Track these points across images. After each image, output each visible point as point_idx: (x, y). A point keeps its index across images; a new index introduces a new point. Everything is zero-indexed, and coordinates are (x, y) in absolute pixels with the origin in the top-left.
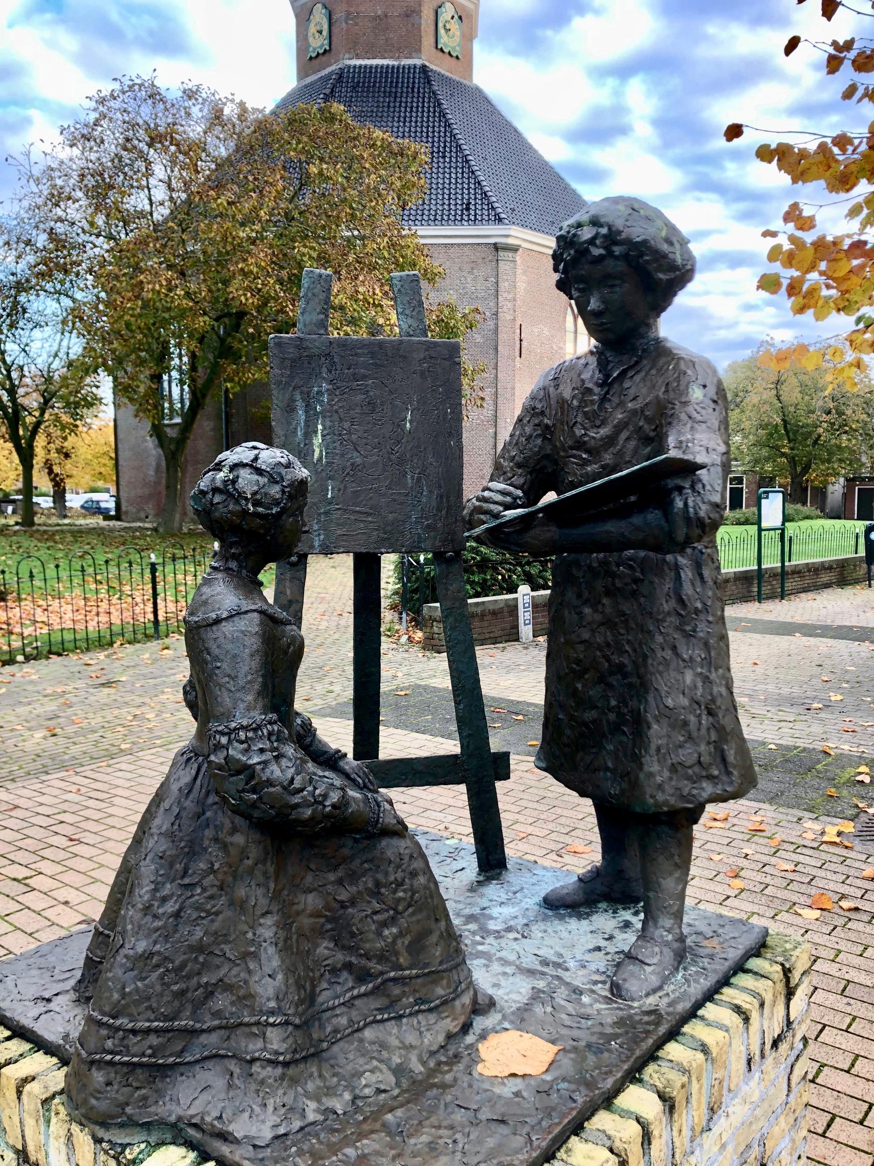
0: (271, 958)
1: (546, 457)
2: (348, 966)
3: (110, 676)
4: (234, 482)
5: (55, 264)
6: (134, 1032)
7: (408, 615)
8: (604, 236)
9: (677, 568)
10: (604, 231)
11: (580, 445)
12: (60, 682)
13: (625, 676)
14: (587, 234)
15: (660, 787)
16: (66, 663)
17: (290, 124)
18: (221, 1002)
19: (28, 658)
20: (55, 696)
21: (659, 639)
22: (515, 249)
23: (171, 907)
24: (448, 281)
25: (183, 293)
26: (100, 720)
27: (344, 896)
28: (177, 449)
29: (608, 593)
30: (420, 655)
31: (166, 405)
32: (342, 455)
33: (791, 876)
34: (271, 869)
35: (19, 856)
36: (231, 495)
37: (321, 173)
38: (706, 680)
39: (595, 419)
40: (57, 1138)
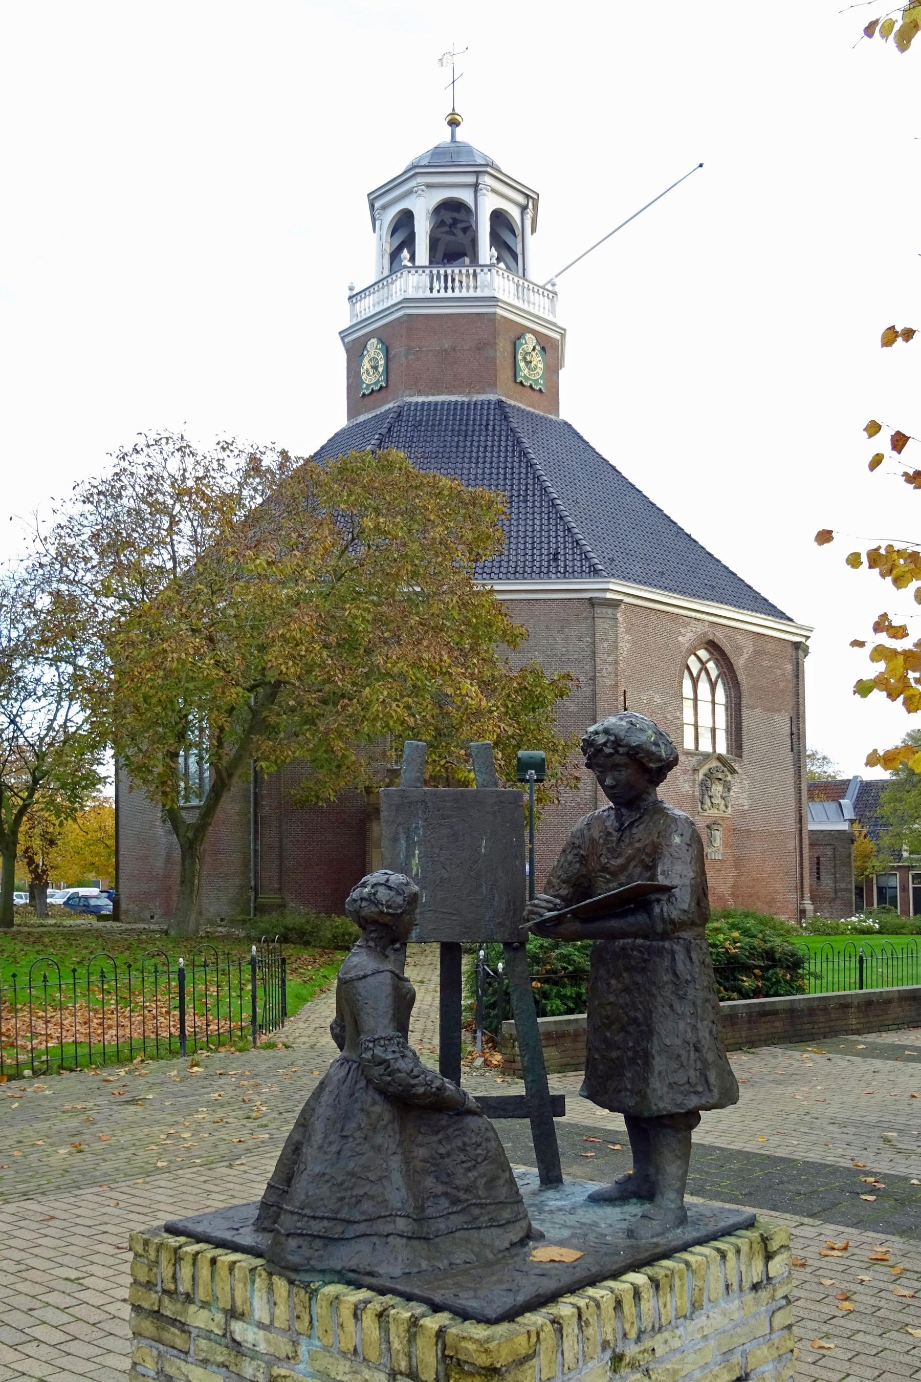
0: (397, 1178)
1: (583, 876)
2: (446, 1194)
3: (134, 1094)
4: (375, 894)
5: (60, 629)
6: (314, 1218)
7: (483, 1034)
8: (613, 742)
9: (673, 953)
10: (612, 738)
11: (604, 869)
12: (79, 1098)
13: (639, 1025)
14: (601, 739)
15: (661, 1098)
16: (81, 1078)
17: (340, 473)
18: (366, 1206)
19: (36, 1073)
20: (74, 1112)
21: (660, 999)
22: (615, 604)
23: (334, 1148)
24: (532, 642)
25: (212, 662)
26: (129, 1137)
27: (442, 1151)
28: (196, 837)
29: (627, 969)
30: (499, 1080)
31: (182, 784)
32: (433, 872)
33: (908, 1301)
34: (397, 1129)
35: (66, 1260)
36: (372, 902)
37: (377, 527)
38: (695, 1028)
39: (614, 853)
40: (260, 1291)
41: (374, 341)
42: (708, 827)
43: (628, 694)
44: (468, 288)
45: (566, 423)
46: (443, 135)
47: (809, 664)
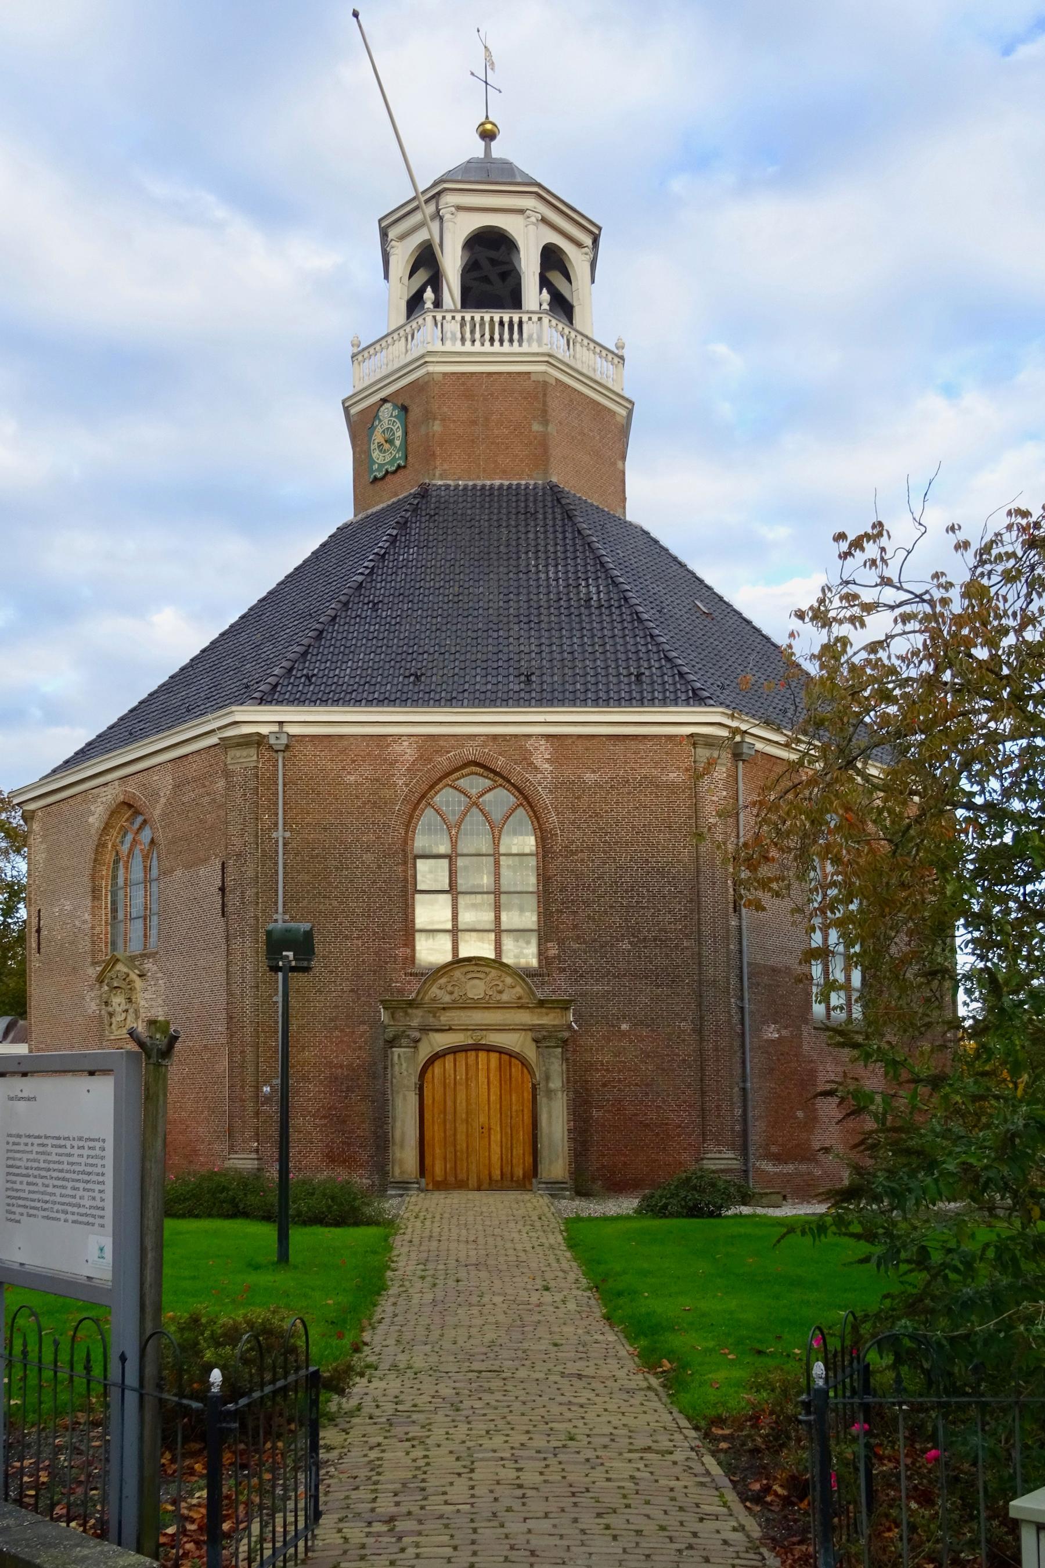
46: (476, 149)
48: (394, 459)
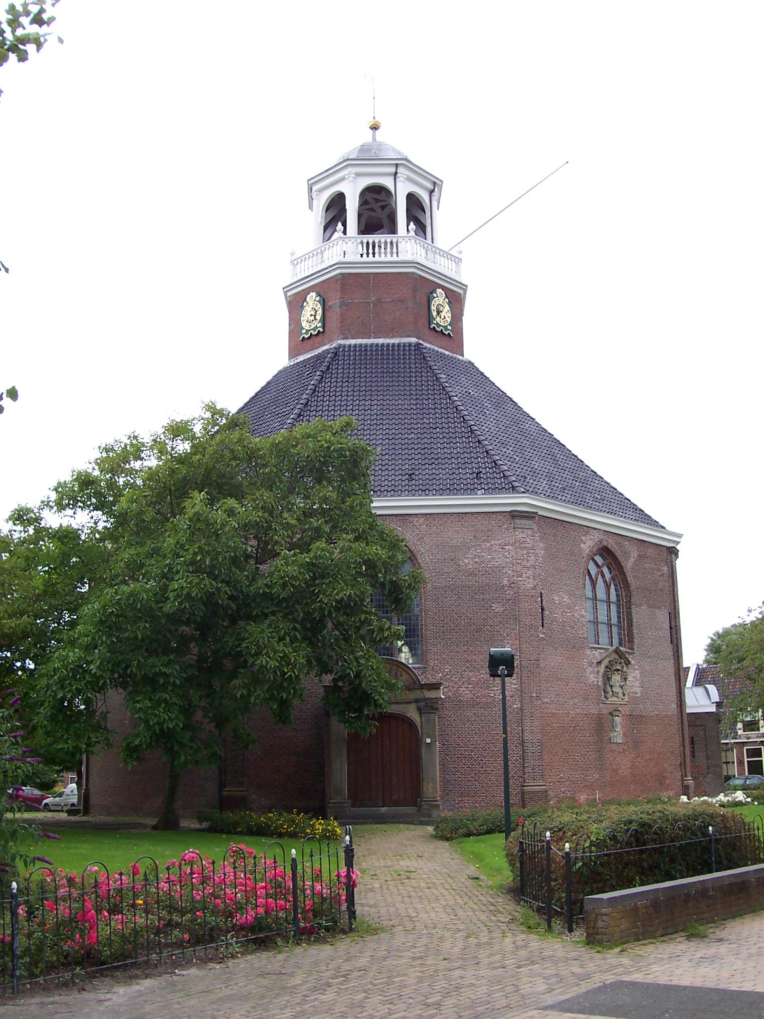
41: (313, 294)
42: (611, 714)
43: (544, 595)
44: (386, 254)
45: (470, 362)
46: (367, 136)
47: (680, 564)
48: (316, 327)
